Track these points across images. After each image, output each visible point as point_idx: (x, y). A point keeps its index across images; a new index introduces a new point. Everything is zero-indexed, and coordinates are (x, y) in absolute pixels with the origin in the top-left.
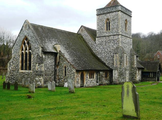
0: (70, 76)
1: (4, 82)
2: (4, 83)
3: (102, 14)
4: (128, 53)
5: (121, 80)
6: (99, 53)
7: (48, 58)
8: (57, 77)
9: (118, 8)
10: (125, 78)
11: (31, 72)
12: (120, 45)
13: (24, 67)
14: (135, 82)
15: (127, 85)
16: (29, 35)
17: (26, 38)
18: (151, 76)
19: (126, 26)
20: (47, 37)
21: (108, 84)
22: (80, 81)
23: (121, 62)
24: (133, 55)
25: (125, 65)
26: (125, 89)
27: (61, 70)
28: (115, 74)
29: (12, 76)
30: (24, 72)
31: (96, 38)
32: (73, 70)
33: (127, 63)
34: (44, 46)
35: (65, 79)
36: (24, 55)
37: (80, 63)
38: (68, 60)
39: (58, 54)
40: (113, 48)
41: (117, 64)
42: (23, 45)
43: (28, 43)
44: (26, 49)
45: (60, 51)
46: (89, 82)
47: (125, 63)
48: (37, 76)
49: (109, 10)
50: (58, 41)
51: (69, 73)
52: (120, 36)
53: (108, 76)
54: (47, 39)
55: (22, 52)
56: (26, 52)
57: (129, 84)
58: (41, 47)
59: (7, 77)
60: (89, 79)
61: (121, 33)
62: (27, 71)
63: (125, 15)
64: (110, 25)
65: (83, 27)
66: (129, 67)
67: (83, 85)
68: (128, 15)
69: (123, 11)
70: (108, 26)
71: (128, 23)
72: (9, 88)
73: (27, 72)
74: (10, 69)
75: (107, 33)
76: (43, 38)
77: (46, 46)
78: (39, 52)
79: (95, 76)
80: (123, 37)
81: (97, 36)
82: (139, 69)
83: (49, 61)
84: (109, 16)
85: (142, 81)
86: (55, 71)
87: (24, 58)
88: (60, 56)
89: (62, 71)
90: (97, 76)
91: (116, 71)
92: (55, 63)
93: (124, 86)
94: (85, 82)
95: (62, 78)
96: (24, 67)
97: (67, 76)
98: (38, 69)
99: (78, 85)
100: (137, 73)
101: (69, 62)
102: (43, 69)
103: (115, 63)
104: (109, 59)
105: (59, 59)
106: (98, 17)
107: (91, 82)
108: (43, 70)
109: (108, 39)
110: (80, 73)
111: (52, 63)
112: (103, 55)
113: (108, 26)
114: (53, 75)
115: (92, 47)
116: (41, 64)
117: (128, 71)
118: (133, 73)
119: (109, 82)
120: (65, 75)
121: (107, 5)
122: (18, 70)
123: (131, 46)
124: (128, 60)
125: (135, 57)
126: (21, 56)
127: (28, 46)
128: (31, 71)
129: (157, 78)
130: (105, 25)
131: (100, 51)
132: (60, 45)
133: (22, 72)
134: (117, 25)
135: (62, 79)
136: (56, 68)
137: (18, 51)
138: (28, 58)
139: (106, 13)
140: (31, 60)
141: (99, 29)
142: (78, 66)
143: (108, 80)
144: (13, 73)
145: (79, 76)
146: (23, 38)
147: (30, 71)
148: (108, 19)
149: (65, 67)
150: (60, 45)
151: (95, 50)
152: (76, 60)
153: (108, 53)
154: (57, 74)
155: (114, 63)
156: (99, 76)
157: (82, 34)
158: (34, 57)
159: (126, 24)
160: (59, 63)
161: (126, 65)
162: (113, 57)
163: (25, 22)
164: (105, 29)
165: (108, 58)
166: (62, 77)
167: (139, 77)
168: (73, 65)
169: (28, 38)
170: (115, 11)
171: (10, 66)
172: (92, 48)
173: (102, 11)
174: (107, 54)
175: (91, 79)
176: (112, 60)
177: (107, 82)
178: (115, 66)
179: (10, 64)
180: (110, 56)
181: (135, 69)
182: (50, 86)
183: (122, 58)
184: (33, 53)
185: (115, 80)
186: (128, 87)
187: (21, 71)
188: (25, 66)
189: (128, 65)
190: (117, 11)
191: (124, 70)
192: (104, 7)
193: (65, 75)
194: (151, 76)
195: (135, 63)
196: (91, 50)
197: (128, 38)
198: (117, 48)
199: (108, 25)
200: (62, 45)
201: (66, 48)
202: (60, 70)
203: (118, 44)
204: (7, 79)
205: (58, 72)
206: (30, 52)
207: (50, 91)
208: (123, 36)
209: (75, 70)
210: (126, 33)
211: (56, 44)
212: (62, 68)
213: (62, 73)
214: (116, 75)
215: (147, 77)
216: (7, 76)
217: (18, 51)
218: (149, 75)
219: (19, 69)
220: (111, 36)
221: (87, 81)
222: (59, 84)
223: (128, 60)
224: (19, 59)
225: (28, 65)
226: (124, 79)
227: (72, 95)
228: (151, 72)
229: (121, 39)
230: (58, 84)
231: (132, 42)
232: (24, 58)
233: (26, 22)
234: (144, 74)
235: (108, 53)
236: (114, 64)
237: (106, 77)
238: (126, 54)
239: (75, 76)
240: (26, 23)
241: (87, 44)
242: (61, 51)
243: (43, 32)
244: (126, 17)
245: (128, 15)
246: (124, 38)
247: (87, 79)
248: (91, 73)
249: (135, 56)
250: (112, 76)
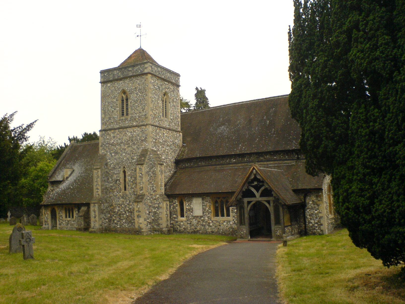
110: (50, 209)
145: (48, 214)
198: (144, 153)
199: (125, 101)
221: (61, 221)
247: (61, 218)
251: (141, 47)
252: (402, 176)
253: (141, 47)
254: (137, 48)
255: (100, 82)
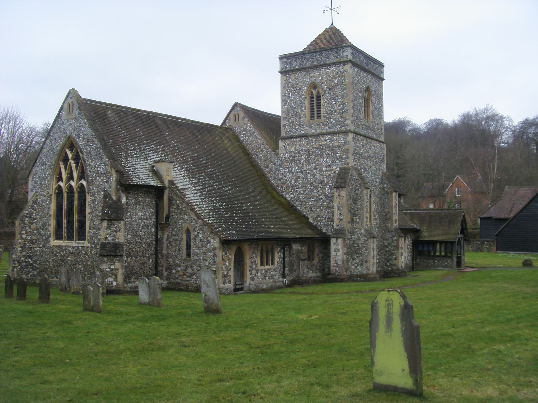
0: (204, 260)
1: (8, 277)
2: (10, 283)
3: (295, 70)
4: (375, 186)
5: (353, 267)
6: (288, 187)
7: (136, 205)
8: (162, 261)
9: (345, 54)
10: (366, 262)
11: (85, 245)
12: (351, 163)
13: (64, 230)
14: (396, 273)
15: (386, 301)
16: (79, 136)
17: (72, 145)
18: (438, 254)
19: (367, 107)
20: (132, 140)
21: (315, 280)
22: (232, 273)
23: (354, 215)
24: (388, 194)
25: (365, 224)
26: (382, 312)
27: (176, 240)
28: (337, 250)
29: (30, 257)
30: (64, 244)
31: (280, 141)
32: (212, 240)
33: (373, 217)
34: (124, 167)
35: (186, 268)
36: (65, 195)
37: (232, 217)
38: (197, 209)
39: (167, 192)
40: (329, 173)
41: (341, 220)
42: (61, 163)
43: (77, 158)
44: (71, 178)
45: (172, 182)
46: (259, 274)
47: (367, 217)
48: (105, 259)
49: (318, 60)
50: (164, 151)
51: (199, 248)
52: (351, 136)
53: (315, 255)
54: (134, 145)
55: (60, 187)
56: (71, 186)
57: (392, 297)
58: (117, 171)
59: (14, 261)
60: (260, 267)
61: (352, 128)
62: (74, 243)
63: (363, 74)
64: (322, 104)
65: (238, 109)
66: (378, 228)
67: (240, 286)
68: (372, 74)
69: (359, 63)
70: (315, 105)
71: (374, 99)
72: (22, 295)
73: (74, 247)
74: (24, 236)
75: (311, 127)
76: (122, 142)
77: (129, 167)
78: (110, 187)
79: (277, 257)
80: (360, 138)
81: (283, 134)
82: (405, 231)
83: (140, 214)
84: (317, 76)
85: (414, 267)
86: (158, 241)
87: (65, 203)
88: (172, 197)
89: (178, 242)
90: (282, 256)
91: (340, 241)
92: (157, 218)
93: (377, 303)
94: (248, 275)
95: (179, 266)
96: (64, 230)
97: (193, 257)
98: (106, 238)
99: (227, 285)
100: (400, 246)
101: (199, 217)
102: (121, 238)
103: (336, 217)
104: (319, 204)
105: (169, 207)
106: (285, 78)
107: (265, 277)
108: (120, 241)
109: (315, 146)
110: (234, 249)
111: (147, 219)
112: (300, 193)
113: (315, 105)
114: (151, 254)
115: (267, 167)
116: (115, 222)
117: (375, 240)
118: (389, 244)
119: (318, 274)
120: (188, 255)
121: (311, 44)
122: (47, 240)
123: (384, 167)
124: (373, 207)
125: (395, 197)
126: (54, 197)
127: (77, 167)
128: (86, 242)
129: (455, 259)
130: (307, 103)
131: (293, 182)
132: (171, 165)
133: (59, 247)
134: (343, 103)
135: (179, 269)
136: (160, 233)
137: (45, 184)
138: (76, 203)
139: (308, 68)
140: (85, 210)
141: (287, 114)
142: (228, 229)
143: (316, 269)
144: (31, 249)
145: (229, 259)
146: (61, 142)
147: (84, 243)
148: (314, 86)
149: (188, 232)
150: (172, 162)
151: (275, 178)
152: (219, 210)
153: (315, 187)
154: (164, 252)
155: (333, 216)
156: (290, 257)
157: (237, 129)
158: (93, 202)
159: (367, 101)
160: (168, 217)
161: (368, 223)
162: (331, 198)
163: (67, 97)
164: (307, 114)
165: (317, 201)
166: (178, 262)
167: (405, 257)
168: (210, 226)
169: (77, 144)
170: (335, 61)
171: (22, 228)
172: (266, 170)
173: (295, 61)
174: (312, 191)
175: (267, 267)
176: (329, 208)
177: (315, 275)
178: (338, 225)
179: (23, 221)
180: (321, 197)
181: (394, 233)
182: (146, 289)
183: (359, 202)
184: (90, 190)
185: (338, 267)
186: (389, 305)
187: (54, 242)
188: (68, 228)
189: (374, 223)
190: (340, 62)
191: (363, 238)
192: (301, 50)
193: (188, 255)
194: (440, 253)
195: (396, 217)
196: (261, 176)
197: (374, 143)
200: (178, 162)
201: (191, 174)
202: (171, 240)
203: (345, 158)
204: (14, 267)
205: (165, 245)
206: (82, 185)
207: (145, 304)
208: (361, 135)
209: (218, 240)
210: (368, 128)
211: (159, 162)
212: (177, 235)
213: (179, 250)
214: (339, 254)
215: (429, 255)
216: (14, 256)
217: (45, 184)
218: (435, 251)
219: (50, 236)
220: (323, 135)
221: (254, 272)
222: (170, 283)
223: (373, 207)
224: (49, 208)
225: (76, 224)
226: (362, 264)
227: (212, 318)
228: (441, 242)
229: (352, 144)
230: (166, 282)
231: (385, 152)
232: (65, 203)
233: (71, 95)
234: (420, 248)
235: (315, 187)
236: (332, 221)
237: (310, 258)
238: (369, 191)
239: (218, 259)
240: (71, 98)
241: (252, 158)
242: (176, 182)
243: (120, 126)
244: (365, 79)
245: (372, 74)
246: (362, 142)
247: (254, 266)
248: (264, 248)
249: (395, 195)
250: (327, 255)
251: (332, 24)
252: (9, 249)
253: (332, 24)
254: (328, 26)
255: (280, 72)
